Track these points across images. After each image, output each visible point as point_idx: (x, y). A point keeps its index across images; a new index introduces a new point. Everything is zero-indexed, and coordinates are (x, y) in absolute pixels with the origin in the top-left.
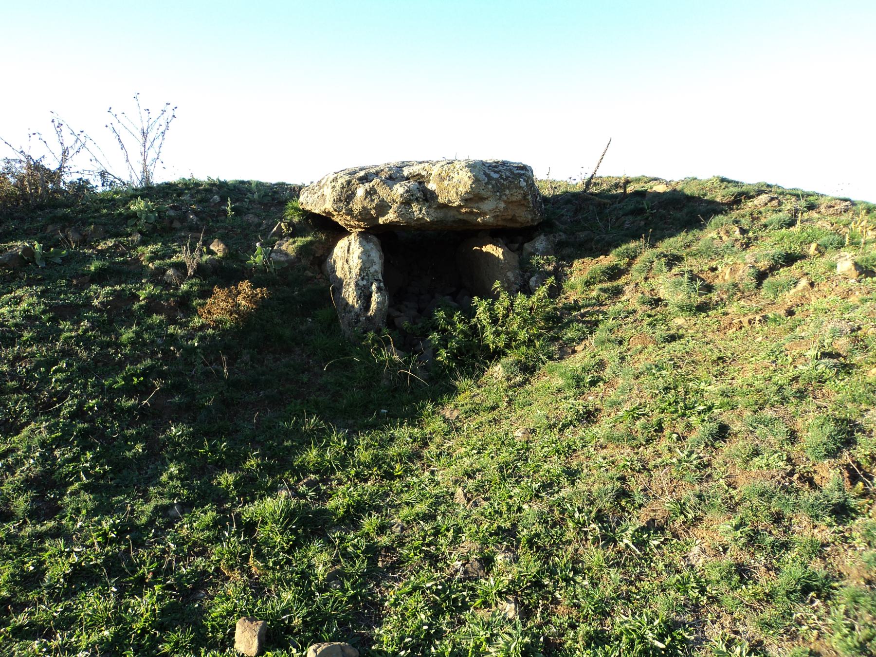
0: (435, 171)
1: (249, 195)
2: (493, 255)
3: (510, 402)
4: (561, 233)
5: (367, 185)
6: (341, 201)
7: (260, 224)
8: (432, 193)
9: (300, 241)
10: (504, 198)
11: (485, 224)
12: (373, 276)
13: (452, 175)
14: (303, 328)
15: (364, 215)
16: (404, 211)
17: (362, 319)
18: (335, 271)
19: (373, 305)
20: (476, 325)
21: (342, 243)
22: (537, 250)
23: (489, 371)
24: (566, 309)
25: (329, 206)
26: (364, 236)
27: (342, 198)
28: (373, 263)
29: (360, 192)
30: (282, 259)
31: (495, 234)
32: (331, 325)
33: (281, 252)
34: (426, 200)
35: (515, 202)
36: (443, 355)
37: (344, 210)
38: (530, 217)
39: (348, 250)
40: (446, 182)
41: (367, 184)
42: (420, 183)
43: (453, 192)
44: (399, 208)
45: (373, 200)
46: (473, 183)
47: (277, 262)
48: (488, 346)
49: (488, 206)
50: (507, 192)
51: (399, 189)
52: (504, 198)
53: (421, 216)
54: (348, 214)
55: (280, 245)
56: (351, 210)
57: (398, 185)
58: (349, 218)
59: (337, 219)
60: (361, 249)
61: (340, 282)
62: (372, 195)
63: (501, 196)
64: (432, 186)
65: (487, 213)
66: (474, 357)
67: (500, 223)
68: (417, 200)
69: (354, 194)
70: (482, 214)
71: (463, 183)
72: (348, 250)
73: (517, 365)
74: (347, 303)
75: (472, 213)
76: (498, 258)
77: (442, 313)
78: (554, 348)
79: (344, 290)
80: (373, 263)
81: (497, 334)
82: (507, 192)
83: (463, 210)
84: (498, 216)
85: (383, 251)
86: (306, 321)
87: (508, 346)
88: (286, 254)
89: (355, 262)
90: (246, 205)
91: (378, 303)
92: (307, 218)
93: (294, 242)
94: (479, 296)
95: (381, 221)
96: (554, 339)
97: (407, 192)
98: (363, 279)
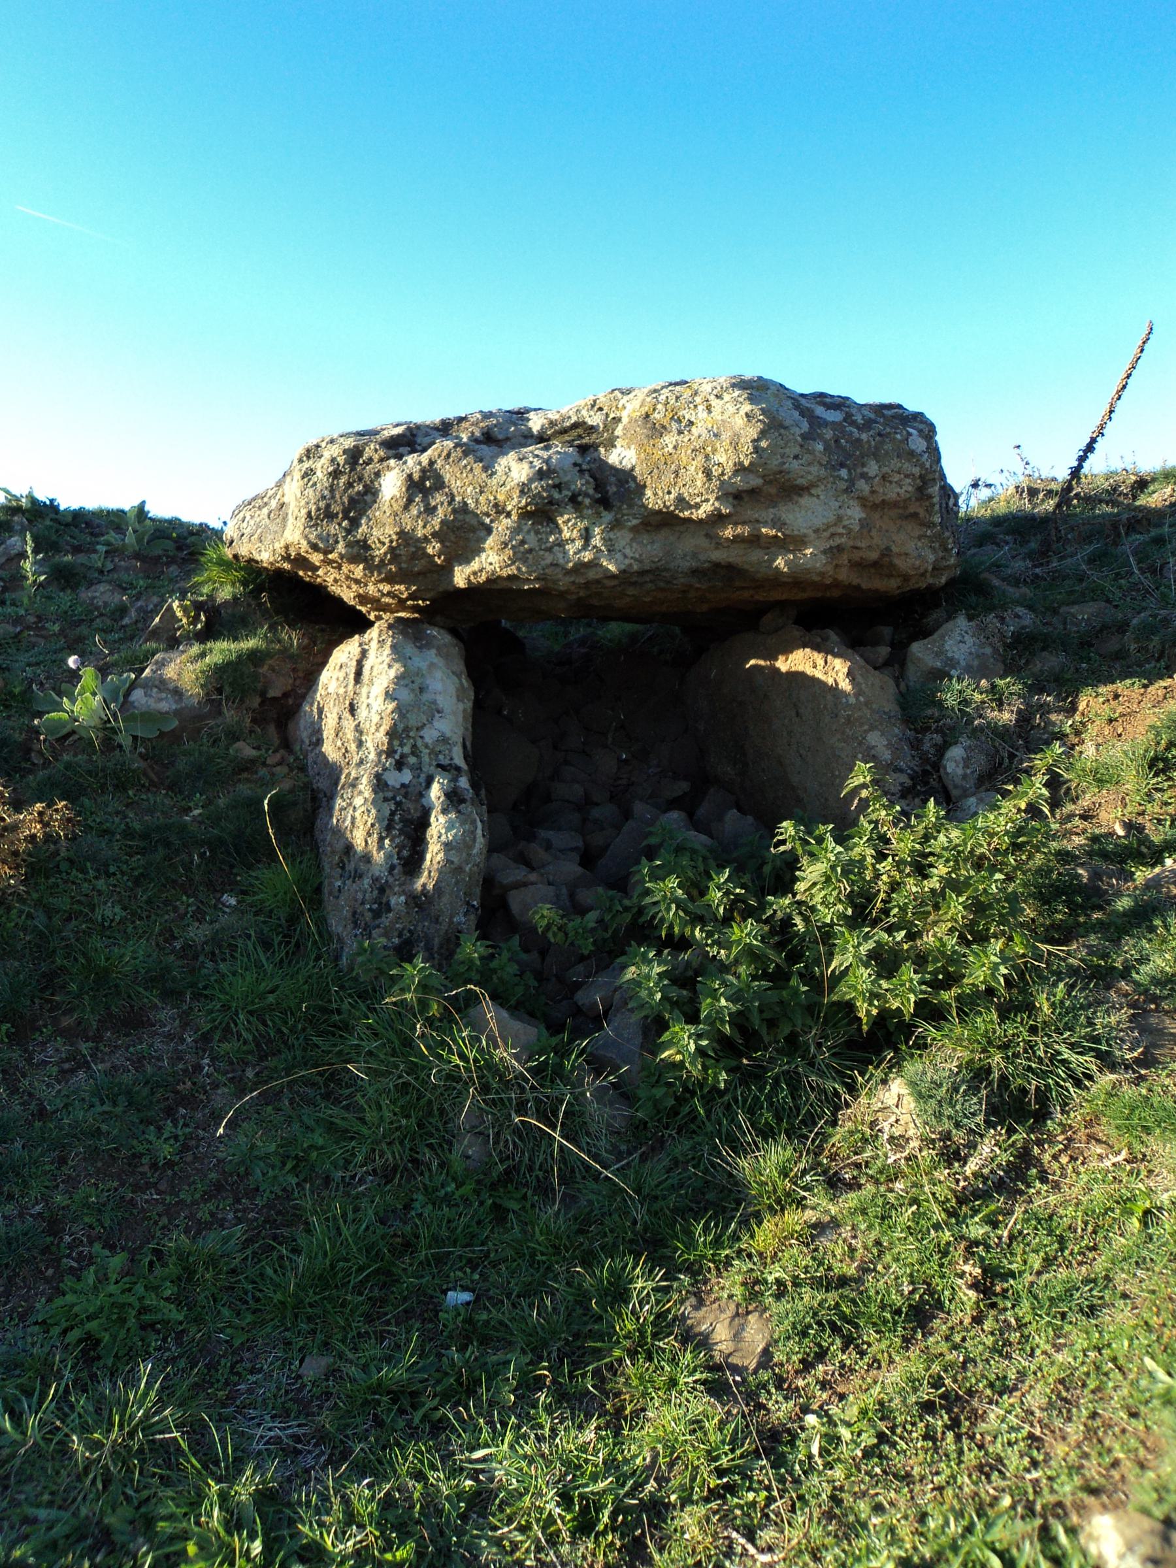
0: (631, 409)
1: (112, 536)
2: (814, 680)
3: (989, 1284)
4: (1020, 610)
5: (413, 463)
6: (329, 515)
7: (123, 610)
8: (625, 477)
9: (221, 650)
10: (863, 486)
11: (797, 580)
12: (434, 753)
13: (688, 415)
14: (198, 933)
15: (406, 559)
16: (532, 541)
17: (397, 901)
18: (320, 742)
19: (434, 854)
20: (787, 922)
21: (345, 653)
22: (952, 663)
23: (861, 1108)
24: (1105, 855)
25: (294, 535)
26: (409, 633)
27: (336, 508)
28: (435, 711)
29: (391, 484)
30: (164, 706)
31: (825, 614)
32: (294, 929)
33: (161, 684)
34: (604, 502)
35: (895, 505)
36: (683, 1044)
37: (341, 547)
38: (931, 558)
39: (358, 674)
40: (669, 440)
41: (411, 460)
42: (583, 449)
43: (693, 469)
44: (516, 531)
45: (430, 510)
46: (763, 434)
47: (149, 717)
48: (850, 1006)
49: (808, 515)
50: (872, 468)
51: (516, 469)
52: (863, 486)
53: (587, 556)
54: (354, 559)
55: (162, 664)
56: (364, 545)
57: (512, 455)
58: (359, 571)
59: (327, 577)
60: (397, 669)
61: (333, 772)
62: (426, 493)
63: (851, 482)
64: (622, 455)
65: (808, 541)
66: (802, 1046)
67: (844, 575)
68: (574, 500)
69: (371, 492)
70: (791, 542)
71: (726, 436)
72: (358, 674)
73: (974, 1089)
74: (349, 848)
75: (755, 540)
76: (834, 690)
77: (672, 882)
78: (1112, 1018)
79: (339, 803)
80: (435, 711)
81: (885, 962)
82: (872, 468)
83: (729, 532)
84: (840, 549)
85: (471, 675)
86: (218, 906)
87: (931, 1012)
88: (177, 693)
89: (376, 710)
90: (97, 560)
91: (447, 846)
92: (259, 590)
93: (203, 655)
94: (799, 821)
95: (460, 577)
96: (1101, 977)
97: (541, 475)
98: (399, 765)
